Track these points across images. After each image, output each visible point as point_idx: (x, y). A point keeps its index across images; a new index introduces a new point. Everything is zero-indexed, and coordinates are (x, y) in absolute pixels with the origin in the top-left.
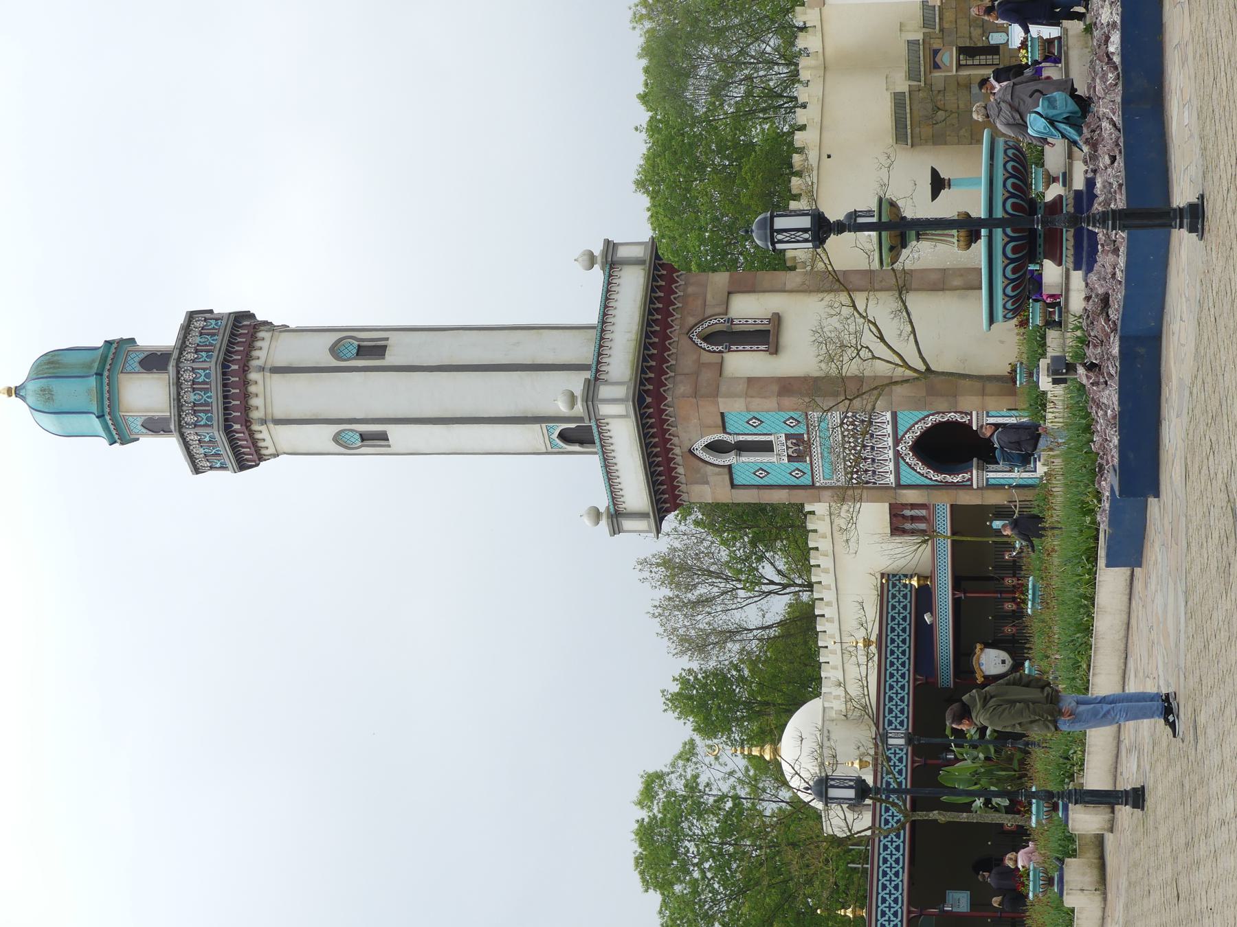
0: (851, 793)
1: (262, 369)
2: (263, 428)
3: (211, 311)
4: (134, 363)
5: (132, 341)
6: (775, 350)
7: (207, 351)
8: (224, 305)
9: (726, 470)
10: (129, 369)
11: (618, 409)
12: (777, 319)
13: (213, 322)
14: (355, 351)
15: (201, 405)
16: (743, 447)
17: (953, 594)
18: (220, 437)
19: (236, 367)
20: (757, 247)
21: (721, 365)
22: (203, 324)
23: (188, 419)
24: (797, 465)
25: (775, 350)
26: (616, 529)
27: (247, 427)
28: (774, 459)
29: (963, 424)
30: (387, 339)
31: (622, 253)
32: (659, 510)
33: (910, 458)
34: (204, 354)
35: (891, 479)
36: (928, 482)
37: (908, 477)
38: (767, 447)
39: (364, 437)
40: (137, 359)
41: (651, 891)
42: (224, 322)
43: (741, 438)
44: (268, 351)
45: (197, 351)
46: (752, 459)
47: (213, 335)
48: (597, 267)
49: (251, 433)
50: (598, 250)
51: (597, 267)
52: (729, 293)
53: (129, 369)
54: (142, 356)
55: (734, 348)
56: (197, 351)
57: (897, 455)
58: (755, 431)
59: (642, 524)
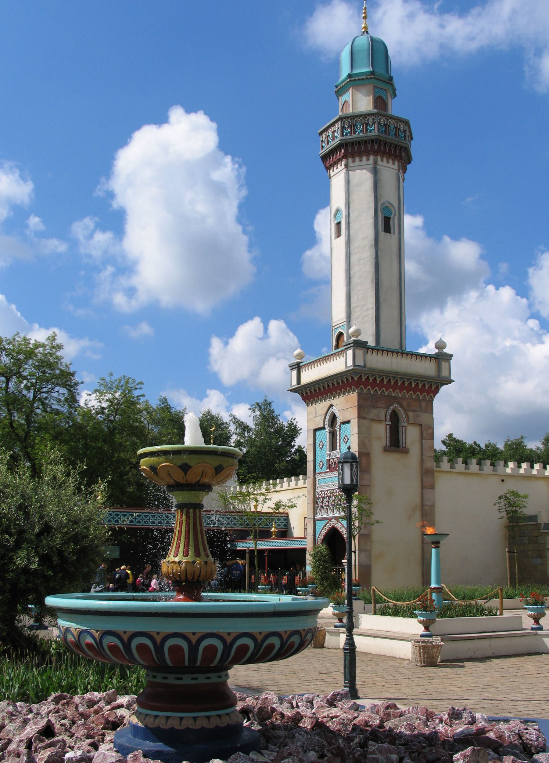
0: (347, 481)
1: (375, 163)
2: (343, 167)
3: (412, 139)
4: (379, 93)
5: (395, 96)
6: (386, 450)
7: (385, 131)
8: (415, 149)
9: (322, 426)
10: (376, 90)
11: (350, 363)
12: (406, 451)
13: (403, 135)
14: (387, 215)
15: (354, 129)
16: (333, 434)
17: (266, 549)
18: (337, 142)
19: (376, 147)
20: (50, 374)
21: (380, 421)
22: (402, 129)
23: (346, 122)
24: (325, 464)
25: (386, 450)
26: (292, 367)
27: (343, 157)
28: (328, 452)
29: (344, 557)
30: (394, 233)
31: (444, 365)
32: (301, 390)
33: (328, 526)
34: (384, 129)
35: (319, 516)
36: (317, 536)
37: (320, 525)
38: (333, 447)
39: (339, 224)
40: (382, 95)
41: (159, 402)
42: (403, 141)
43: (338, 433)
44: (389, 169)
45: (385, 125)
46: (328, 440)
47: (395, 135)
48: (437, 351)
49: (340, 160)
50: (447, 351)
51: (437, 351)
52: (421, 425)
53: (376, 90)
54: (384, 98)
55: (388, 427)
56: (385, 125)
57: (330, 519)
58: (342, 440)
59: (294, 382)
